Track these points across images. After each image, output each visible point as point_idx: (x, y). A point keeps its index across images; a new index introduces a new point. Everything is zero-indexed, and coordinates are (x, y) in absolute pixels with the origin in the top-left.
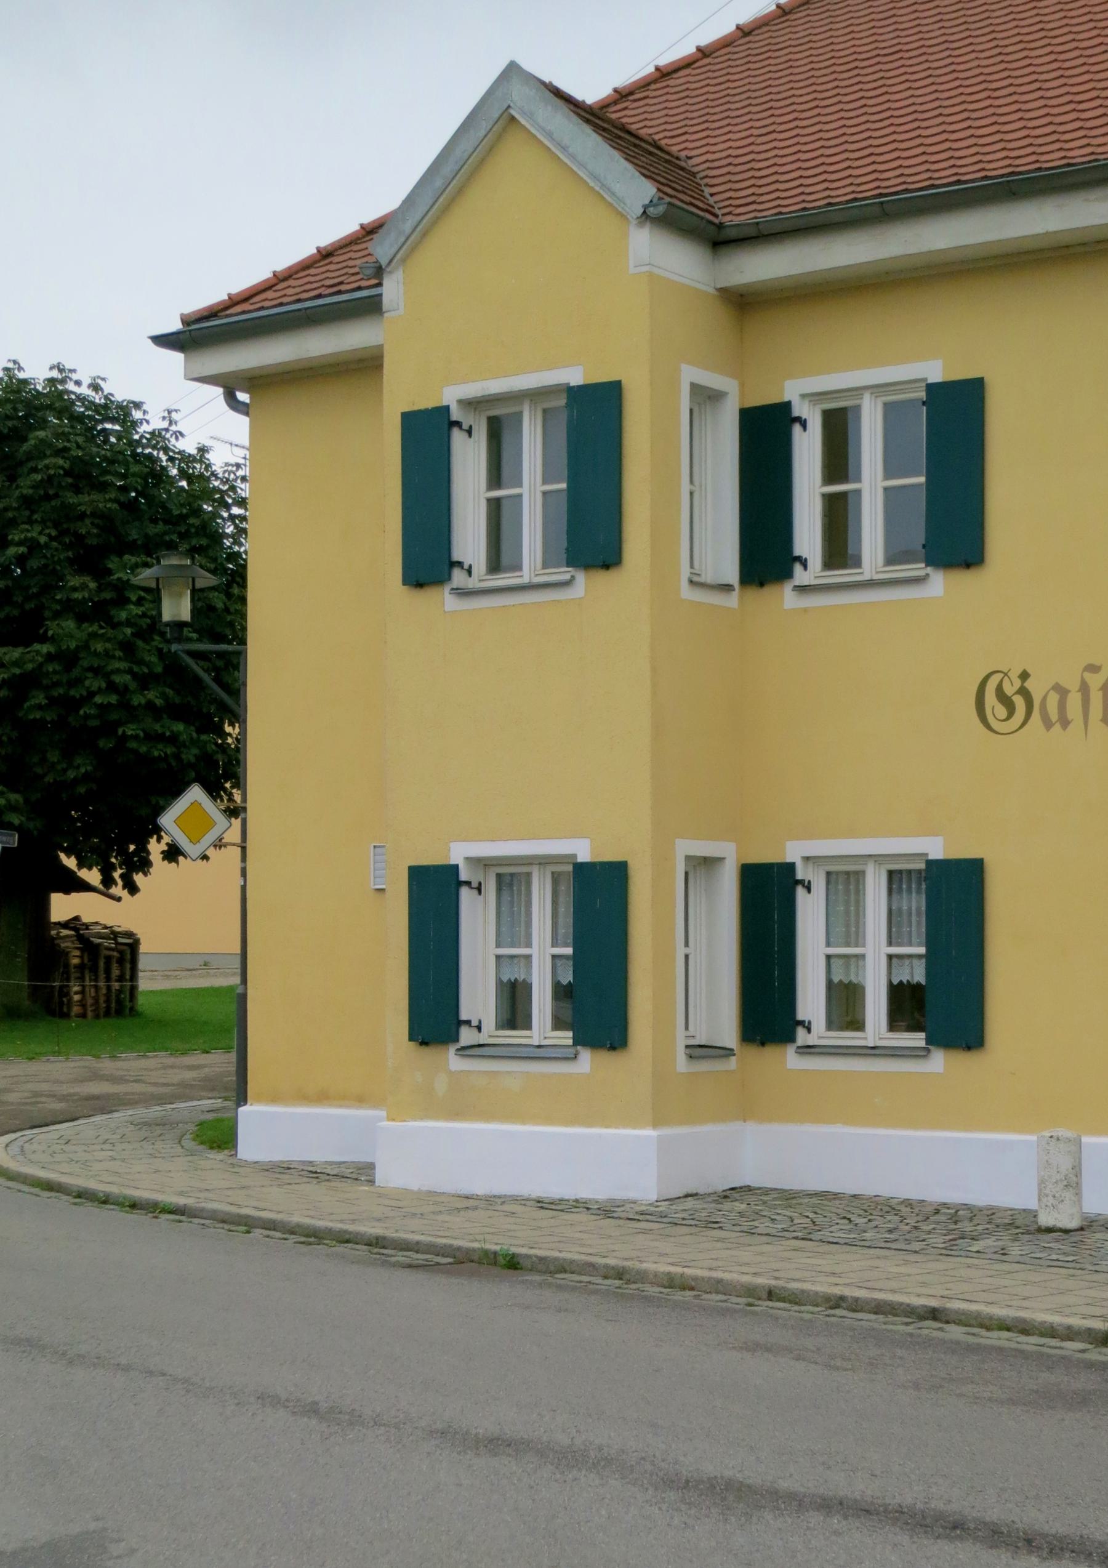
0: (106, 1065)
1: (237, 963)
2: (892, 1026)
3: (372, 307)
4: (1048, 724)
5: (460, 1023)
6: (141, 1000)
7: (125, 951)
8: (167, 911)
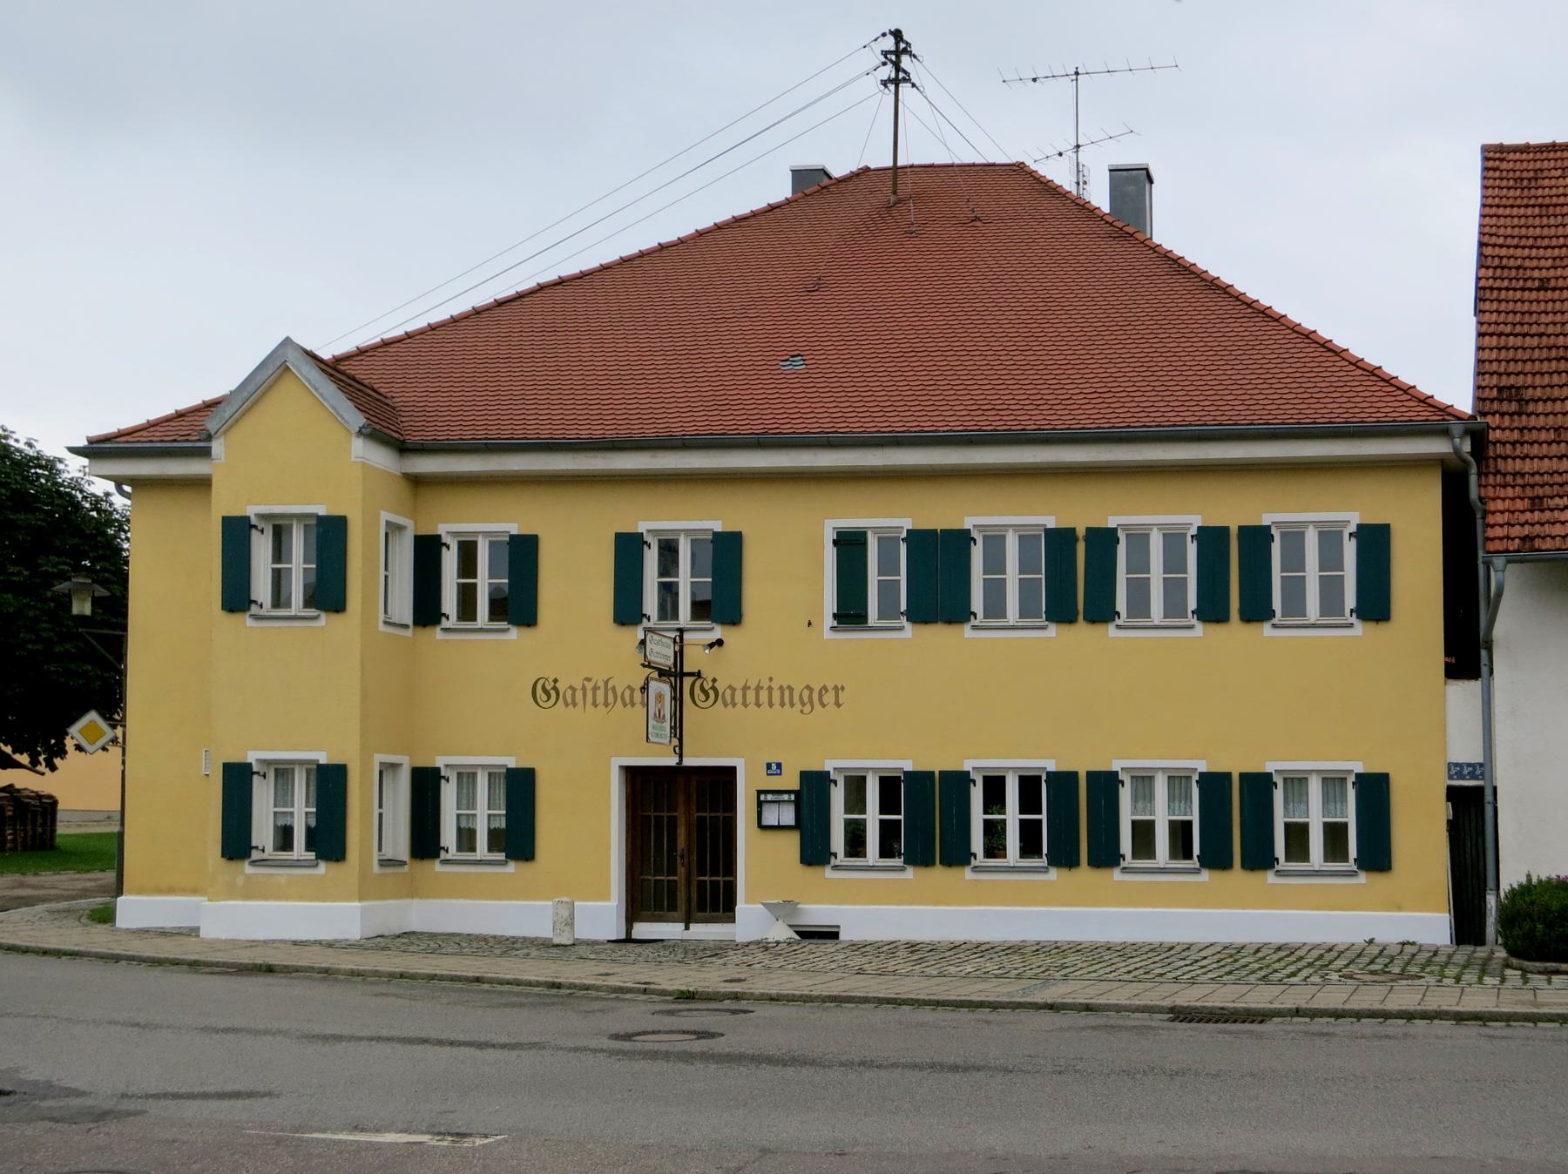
0: (31, 879)
1: (118, 817)
2: (490, 850)
3: (205, 453)
4: (567, 705)
5: (252, 848)
6: (58, 840)
7: (48, 807)
8: (77, 781)
